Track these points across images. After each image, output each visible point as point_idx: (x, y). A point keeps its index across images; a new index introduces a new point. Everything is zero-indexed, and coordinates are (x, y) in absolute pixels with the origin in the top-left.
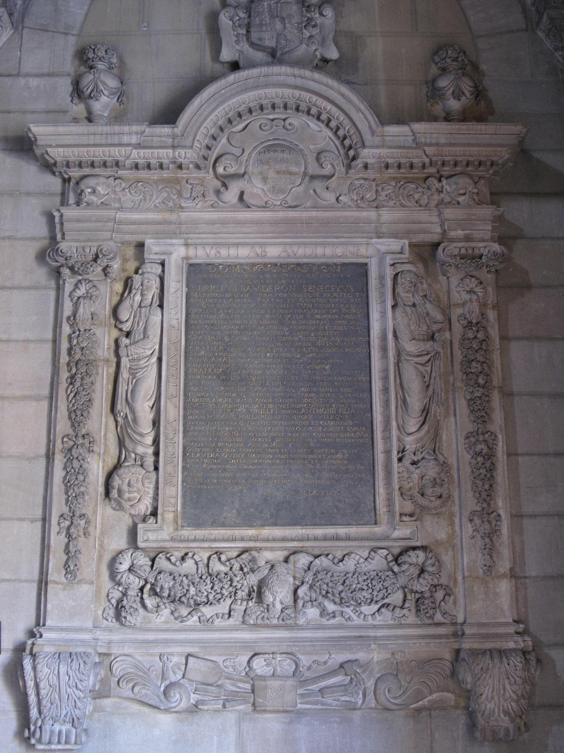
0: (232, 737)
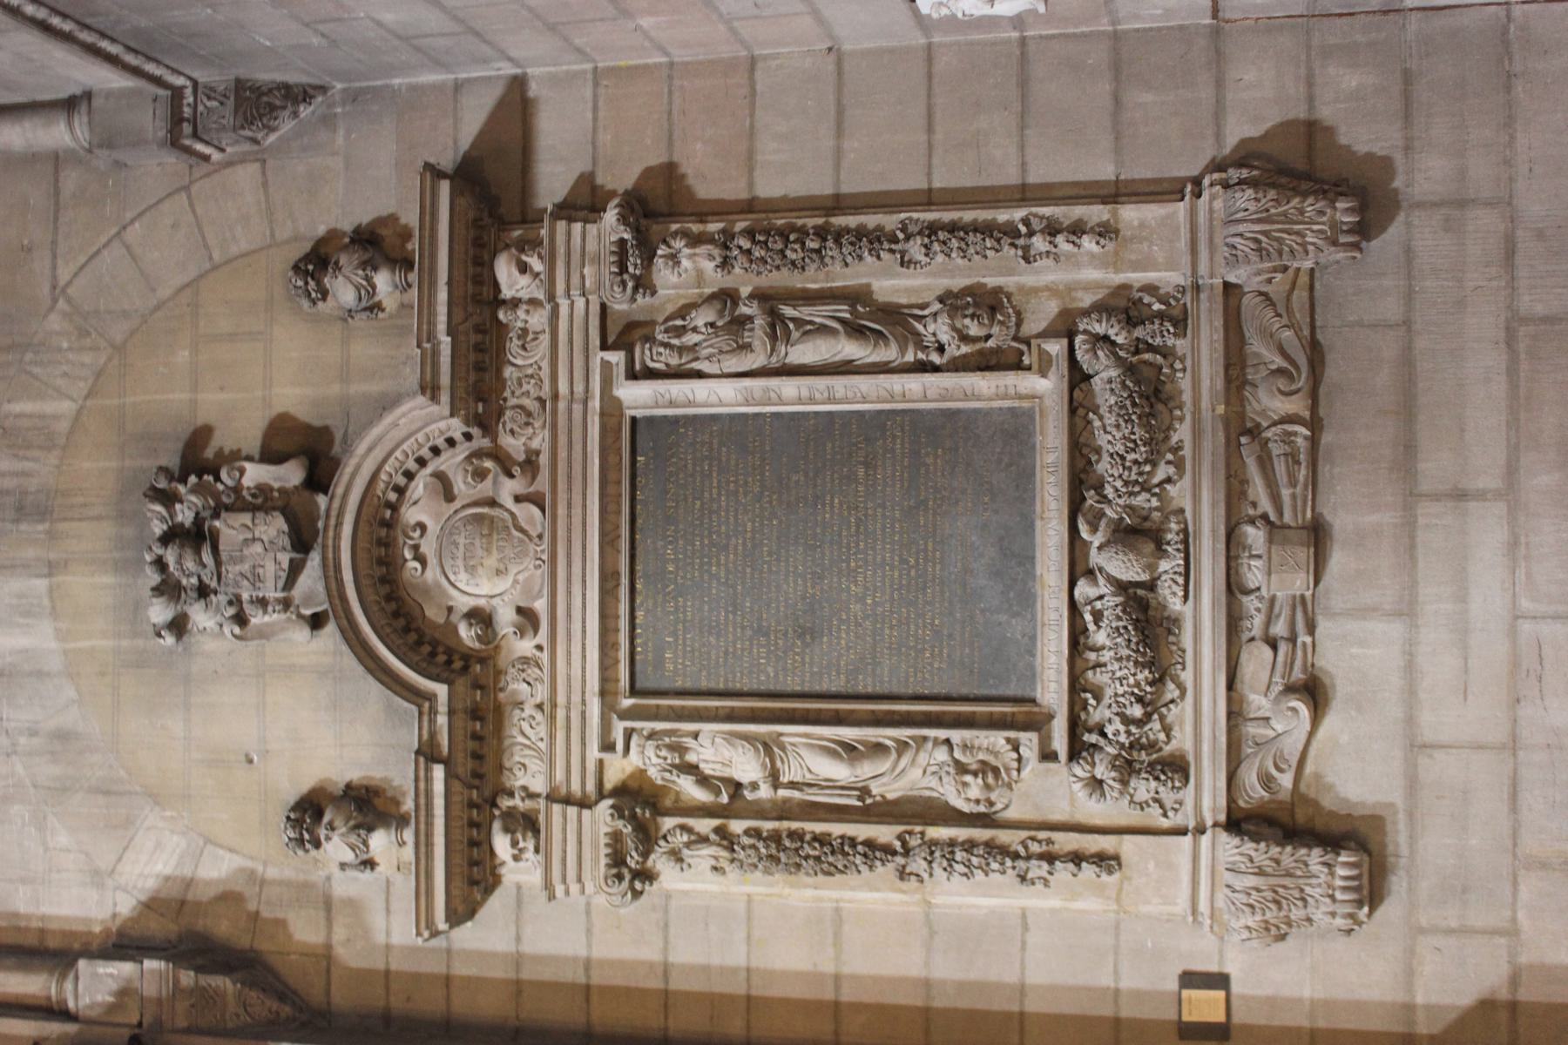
0: (1352, 626)
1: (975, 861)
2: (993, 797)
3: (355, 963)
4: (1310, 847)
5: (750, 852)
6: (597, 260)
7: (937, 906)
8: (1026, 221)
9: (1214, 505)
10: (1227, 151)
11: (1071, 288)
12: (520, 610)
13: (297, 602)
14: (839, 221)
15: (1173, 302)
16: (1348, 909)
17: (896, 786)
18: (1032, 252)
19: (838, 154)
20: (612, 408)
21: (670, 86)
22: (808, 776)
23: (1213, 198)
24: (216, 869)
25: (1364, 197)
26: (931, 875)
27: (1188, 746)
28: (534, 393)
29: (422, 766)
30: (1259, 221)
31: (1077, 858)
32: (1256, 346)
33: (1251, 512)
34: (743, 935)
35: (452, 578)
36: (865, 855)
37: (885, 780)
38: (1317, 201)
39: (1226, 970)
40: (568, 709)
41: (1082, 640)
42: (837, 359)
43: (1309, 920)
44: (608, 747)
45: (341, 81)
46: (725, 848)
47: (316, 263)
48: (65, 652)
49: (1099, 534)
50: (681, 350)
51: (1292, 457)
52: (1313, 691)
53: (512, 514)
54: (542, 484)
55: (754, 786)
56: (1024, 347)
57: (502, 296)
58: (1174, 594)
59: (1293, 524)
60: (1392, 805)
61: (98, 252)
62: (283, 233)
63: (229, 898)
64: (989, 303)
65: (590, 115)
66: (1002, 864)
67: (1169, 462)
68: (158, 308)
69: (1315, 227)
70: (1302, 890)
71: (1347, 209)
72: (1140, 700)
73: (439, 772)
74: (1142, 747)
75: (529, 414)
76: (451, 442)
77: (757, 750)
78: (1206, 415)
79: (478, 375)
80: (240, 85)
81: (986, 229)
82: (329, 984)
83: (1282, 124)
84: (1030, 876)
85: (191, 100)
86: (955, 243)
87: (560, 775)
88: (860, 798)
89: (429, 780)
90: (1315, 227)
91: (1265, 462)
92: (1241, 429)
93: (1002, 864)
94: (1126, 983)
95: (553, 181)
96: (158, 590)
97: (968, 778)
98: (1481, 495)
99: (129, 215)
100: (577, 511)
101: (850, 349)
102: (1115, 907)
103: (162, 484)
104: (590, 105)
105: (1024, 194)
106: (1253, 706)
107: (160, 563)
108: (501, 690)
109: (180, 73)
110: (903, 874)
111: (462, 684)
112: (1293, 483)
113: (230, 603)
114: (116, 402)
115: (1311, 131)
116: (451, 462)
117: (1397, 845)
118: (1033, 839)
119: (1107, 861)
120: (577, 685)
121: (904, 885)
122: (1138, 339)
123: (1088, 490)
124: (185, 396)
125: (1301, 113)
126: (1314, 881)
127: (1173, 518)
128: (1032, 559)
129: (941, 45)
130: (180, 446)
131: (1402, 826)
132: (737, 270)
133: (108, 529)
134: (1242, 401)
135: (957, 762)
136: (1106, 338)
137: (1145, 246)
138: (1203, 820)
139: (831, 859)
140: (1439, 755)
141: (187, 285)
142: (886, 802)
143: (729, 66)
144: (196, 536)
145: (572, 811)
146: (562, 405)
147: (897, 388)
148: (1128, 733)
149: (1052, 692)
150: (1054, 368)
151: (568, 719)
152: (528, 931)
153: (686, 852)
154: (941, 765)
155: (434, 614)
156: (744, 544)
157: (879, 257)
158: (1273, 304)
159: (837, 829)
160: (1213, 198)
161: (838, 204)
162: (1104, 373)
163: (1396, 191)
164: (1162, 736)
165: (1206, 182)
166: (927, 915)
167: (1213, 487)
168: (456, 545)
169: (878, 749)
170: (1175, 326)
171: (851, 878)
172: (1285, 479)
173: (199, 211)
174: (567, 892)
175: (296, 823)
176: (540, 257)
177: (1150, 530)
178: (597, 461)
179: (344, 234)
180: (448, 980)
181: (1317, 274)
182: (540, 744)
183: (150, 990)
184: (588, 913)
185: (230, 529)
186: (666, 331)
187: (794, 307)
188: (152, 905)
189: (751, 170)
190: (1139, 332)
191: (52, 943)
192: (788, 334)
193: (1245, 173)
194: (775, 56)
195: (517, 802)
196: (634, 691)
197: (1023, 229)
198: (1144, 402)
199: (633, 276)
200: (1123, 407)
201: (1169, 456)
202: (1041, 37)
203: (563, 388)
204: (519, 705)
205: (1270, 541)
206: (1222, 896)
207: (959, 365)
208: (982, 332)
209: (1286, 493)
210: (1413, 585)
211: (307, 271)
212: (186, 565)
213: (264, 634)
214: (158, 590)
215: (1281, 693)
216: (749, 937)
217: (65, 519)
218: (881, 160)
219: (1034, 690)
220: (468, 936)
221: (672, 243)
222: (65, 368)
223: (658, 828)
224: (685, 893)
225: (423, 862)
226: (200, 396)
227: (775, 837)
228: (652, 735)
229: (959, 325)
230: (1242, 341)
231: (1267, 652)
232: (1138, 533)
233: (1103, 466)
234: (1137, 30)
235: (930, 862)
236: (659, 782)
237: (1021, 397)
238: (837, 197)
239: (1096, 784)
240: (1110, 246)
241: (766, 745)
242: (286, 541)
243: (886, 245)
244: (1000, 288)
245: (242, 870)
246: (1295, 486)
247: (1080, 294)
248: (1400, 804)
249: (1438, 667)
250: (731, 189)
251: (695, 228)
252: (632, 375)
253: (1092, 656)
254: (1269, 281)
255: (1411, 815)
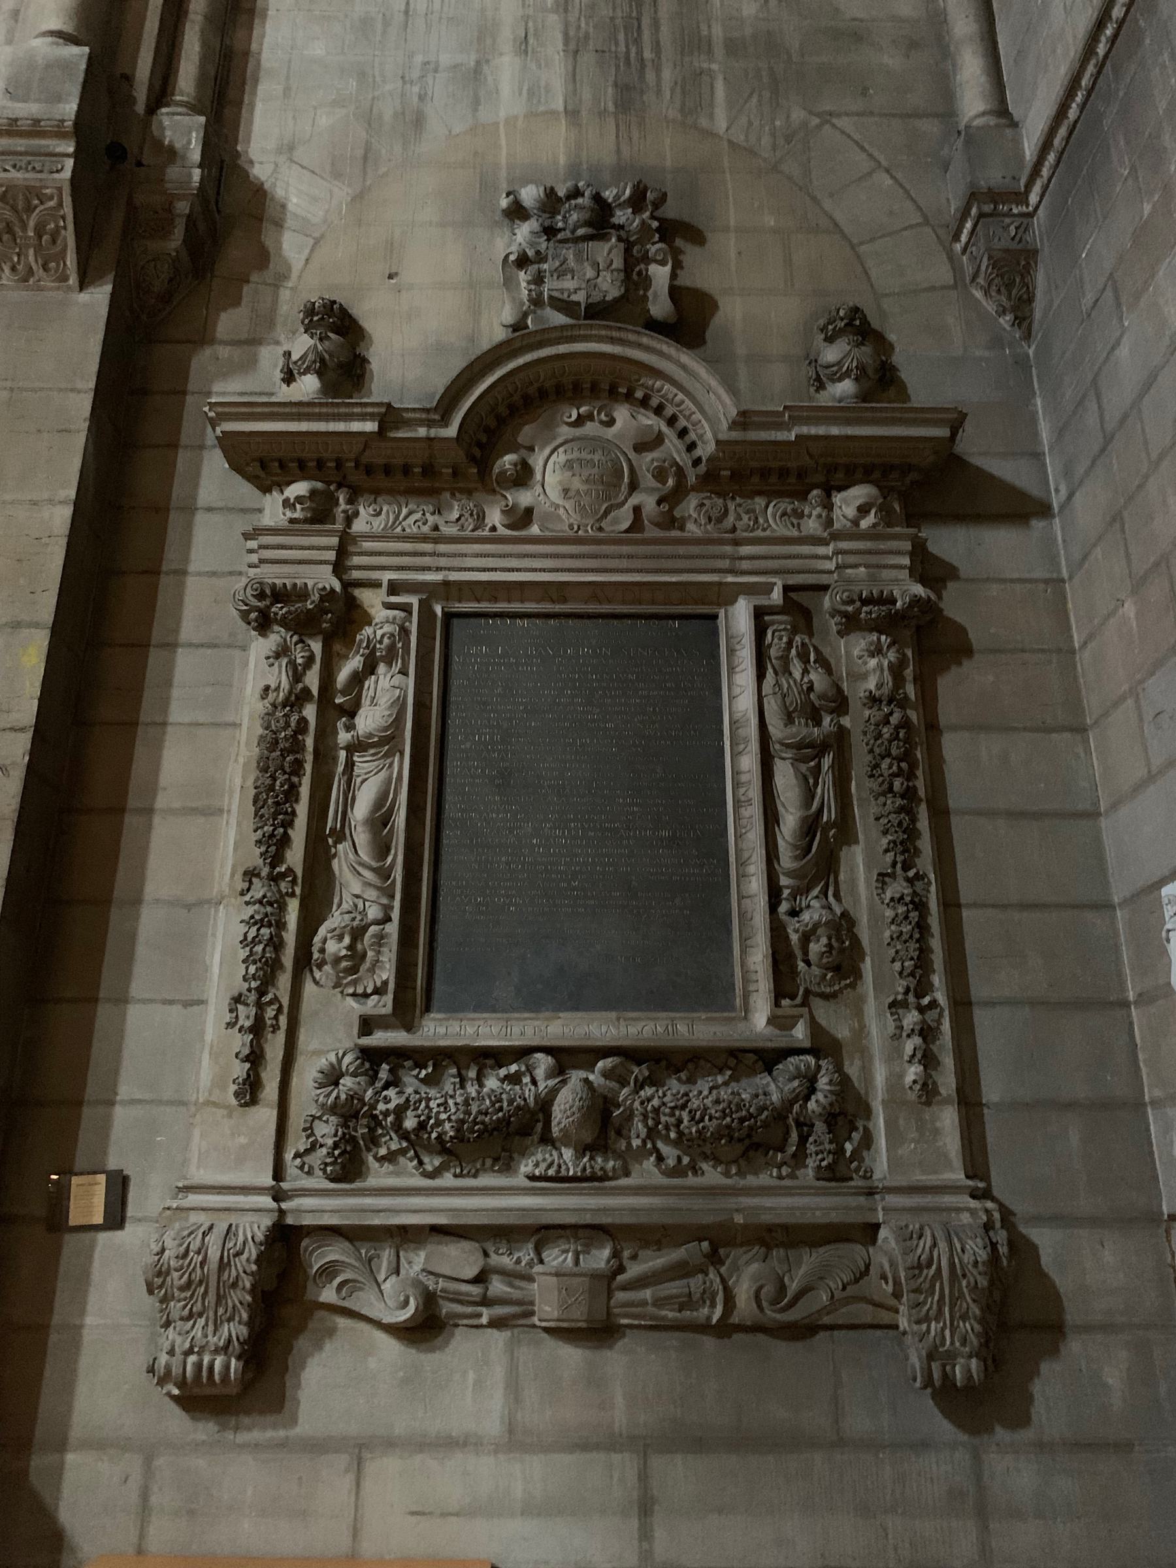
0: (499, 1372)
1: (259, 948)
2: (327, 968)
3: (195, 364)
4: (250, 1324)
5: (282, 723)
6: (873, 579)
7: (217, 911)
8: (933, 1004)
9: (633, 1210)
10: (1023, 1230)
11: (864, 1053)
12: (529, 511)
13: (539, 312)
14: (923, 812)
15: (855, 1164)
16: (176, 1371)
17: (345, 868)
18: (900, 1011)
19: (992, 814)
20: (727, 596)
21: (1049, 651)
22: (359, 780)
23: (973, 1212)
24: (291, 247)
25: (984, 1398)
26: (247, 903)
27: (372, 1182)
28: (739, 525)
29: (376, 410)
30: (952, 1265)
31: (255, 1058)
32: (808, 1262)
33: (626, 1254)
34: (201, 720)
35: (561, 450)
36: (272, 836)
37: (351, 856)
38: (977, 1335)
39: (129, 1227)
40: (433, 554)
41: (489, 1062)
42: (780, 808)
43: (167, 1324)
44: (394, 588)
45: (1036, 353)
46: (287, 699)
47: (858, 326)
48: (497, 124)
49: (602, 1080)
50: (785, 659)
51: (687, 1302)
52: (426, 1327)
53: (623, 503)
54: (651, 532)
55: (350, 727)
56: (799, 1000)
57: (834, 493)
58: (537, 1165)
59: (612, 1302)
60: (294, 1421)
61: (862, 148)
62: (886, 304)
63: (263, 258)
64: (845, 964)
65: (1016, 576)
66: (254, 978)
67: (679, 1159)
68: (814, 199)
69: (947, 1333)
70: (200, 1315)
71: (969, 1371)
72: (422, 1126)
73: (370, 426)
74: (372, 1130)
75: (720, 520)
76: (691, 447)
77: (386, 729)
78: (732, 1202)
79: (761, 470)
80: (1032, 254)
81: (923, 962)
82: (178, 342)
83: (1058, 1295)
84: (240, 1007)
85: (1015, 211)
86: (906, 928)
87: (368, 545)
88: (333, 830)
89: (363, 417)
90: (947, 1333)
91: (681, 1270)
92: (719, 1242)
93: (254, 978)
94: (119, 1112)
95: (948, 542)
96: (551, 193)
97: (347, 940)
98: (645, 1534)
99: (899, 176)
100: (624, 564)
101: (790, 821)
102: (201, 1100)
103: (650, 196)
104: (1027, 576)
105: (962, 1004)
106: (411, 1255)
107: (576, 193)
108: (453, 495)
109: (1042, 196)
110: (250, 875)
111: (459, 455)
112: (658, 1302)
113: (538, 253)
114: (726, 164)
115: (1051, 1328)
116: (673, 447)
117: (249, 1429)
118: (280, 1010)
119: (250, 1092)
120: (456, 562)
121: (239, 876)
122: (813, 1125)
123: (648, 1068)
124: (732, 223)
125: (1072, 1316)
126: (211, 1328)
127: (619, 1163)
128: (576, 1009)
129: (1113, 918)
130: (687, 219)
131: (270, 1434)
132: (867, 713)
133: (609, 159)
134: (748, 1243)
135: (365, 928)
136: (812, 1090)
137: (914, 1135)
138: (290, 1198)
139: (270, 801)
140: (349, 1480)
141: (836, 225)
142: (330, 858)
143: (1074, 703)
144: (600, 219)
145: (331, 555)
146: (728, 549)
147: (752, 869)
148: (386, 1114)
149: (438, 1030)
150: (778, 1032)
151: (423, 554)
152: (216, 518)
153: (284, 661)
154: (364, 913)
155: (526, 433)
156: (594, 721)
157: (887, 851)
158: (857, 1281)
159: (302, 809)
160: (973, 1212)
161: (940, 814)
162: (775, 1088)
163: (990, 1430)
164: (383, 1151)
165: (990, 1205)
166: (209, 902)
167: (650, 1210)
168: (593, 452)
169: (382, 849)
170: (829, 1166)
171: (249, 823)
172: (663, 1294)
173: (905, 233)
174: (251, 551)
175: (330, 306)
176: (874, 525)
177: (606, 1138)
178: (674, 579)
179: (890, 356)
180: (174, 446)
181: (891, 1333)
182: (399, 529)
183: (173, 172)
184: (231, 573)
185: (608, 251)
186: (803, 644)
187: (832, 767)
188: (259, 193)
189: (969, 728)
190: (820, 1127)
191: (228, 112)
192: (805, 760)
193: (1003, 1250)
194: (1088, 751)
195: (343, 506)
196: (448, 616)
197: (926, 1001)
198: (744, 1132)
199: (859, 611)
200: (739, 1108)
201: (686, 1160)
202: (1131, 1024)
203: (746, 550)
204: (438, 511)
205: (595, 1276)
206: (203, 1219)
207: (777, 932)
208: (812, 957)
209: (647, 1294)
210: (546, 1449)
211: (855, 319)
212: (573, 217)
213: (509, 283)
214: (551, 193)
215: (426, 1287)
216: (198, 724)
217: (617, 126)
218: (986, 858)
219: (439, 1011)
220: (215, 464)
221: (893, 650)
222: (756, 123)
223: (312, 636)
224: (247, 664)
225: (281, 410)
226: (732, 235)
227: (297, 746)
228: (404, 631)
229: (819, 931)
230: (814, 1244)
231: (471, 1272)
232: (603, 1126)
233: (674, 1086)
234: (1148, 1130)
235: (260, 902)
236: (358, 637)
237: (746, 996)
238: (946, 812)
239: (332, 1077)
240: (912, 1096)
241: (392, 738)
242: (596, 297)
243: (900, 858)
244: (861, 977)
245: (289, 269)
246: (654, 1304)
247: (857, 1063)
248: (298, 1430)
249: (449, 1479)
250: (947, 712)
251: (909, 672)
252: (759, 614)
253: (472, 1074)
254: (884, 1277)
255: (283, 1445)
